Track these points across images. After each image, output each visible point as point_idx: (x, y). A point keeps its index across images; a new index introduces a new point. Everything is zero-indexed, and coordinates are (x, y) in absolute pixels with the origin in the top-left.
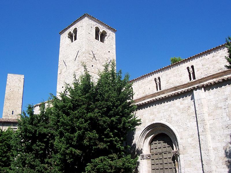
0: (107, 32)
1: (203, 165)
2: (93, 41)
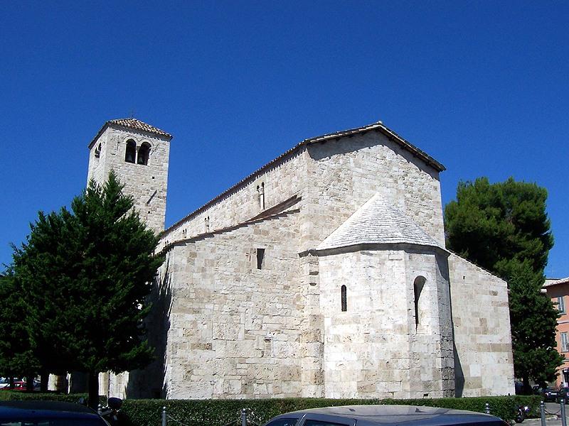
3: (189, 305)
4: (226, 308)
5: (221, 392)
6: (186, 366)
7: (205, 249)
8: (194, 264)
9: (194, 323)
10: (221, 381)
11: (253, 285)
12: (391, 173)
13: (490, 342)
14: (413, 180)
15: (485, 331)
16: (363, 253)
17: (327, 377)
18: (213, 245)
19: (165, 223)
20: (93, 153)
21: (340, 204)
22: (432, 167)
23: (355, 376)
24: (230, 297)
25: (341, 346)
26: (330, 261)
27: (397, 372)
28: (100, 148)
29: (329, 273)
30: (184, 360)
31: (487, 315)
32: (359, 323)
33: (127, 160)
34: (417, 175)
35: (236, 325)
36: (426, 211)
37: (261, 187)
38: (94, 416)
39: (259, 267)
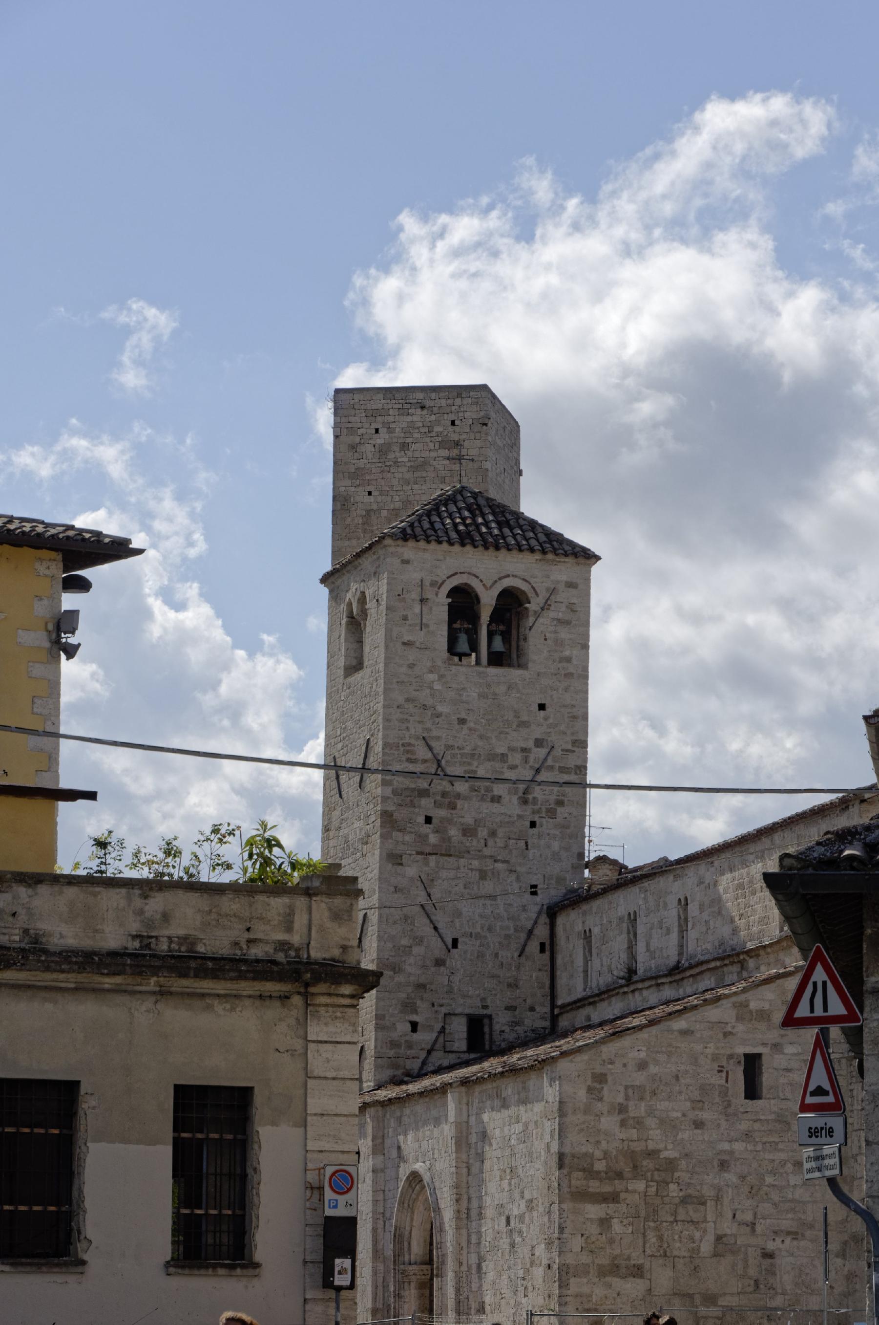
0: (524, 587)
3: (595, 1186)
7: (625, 1065)
8: (601, 1099)
9: (605, 1223)
18: (643, 1055)
33: (452, 649)
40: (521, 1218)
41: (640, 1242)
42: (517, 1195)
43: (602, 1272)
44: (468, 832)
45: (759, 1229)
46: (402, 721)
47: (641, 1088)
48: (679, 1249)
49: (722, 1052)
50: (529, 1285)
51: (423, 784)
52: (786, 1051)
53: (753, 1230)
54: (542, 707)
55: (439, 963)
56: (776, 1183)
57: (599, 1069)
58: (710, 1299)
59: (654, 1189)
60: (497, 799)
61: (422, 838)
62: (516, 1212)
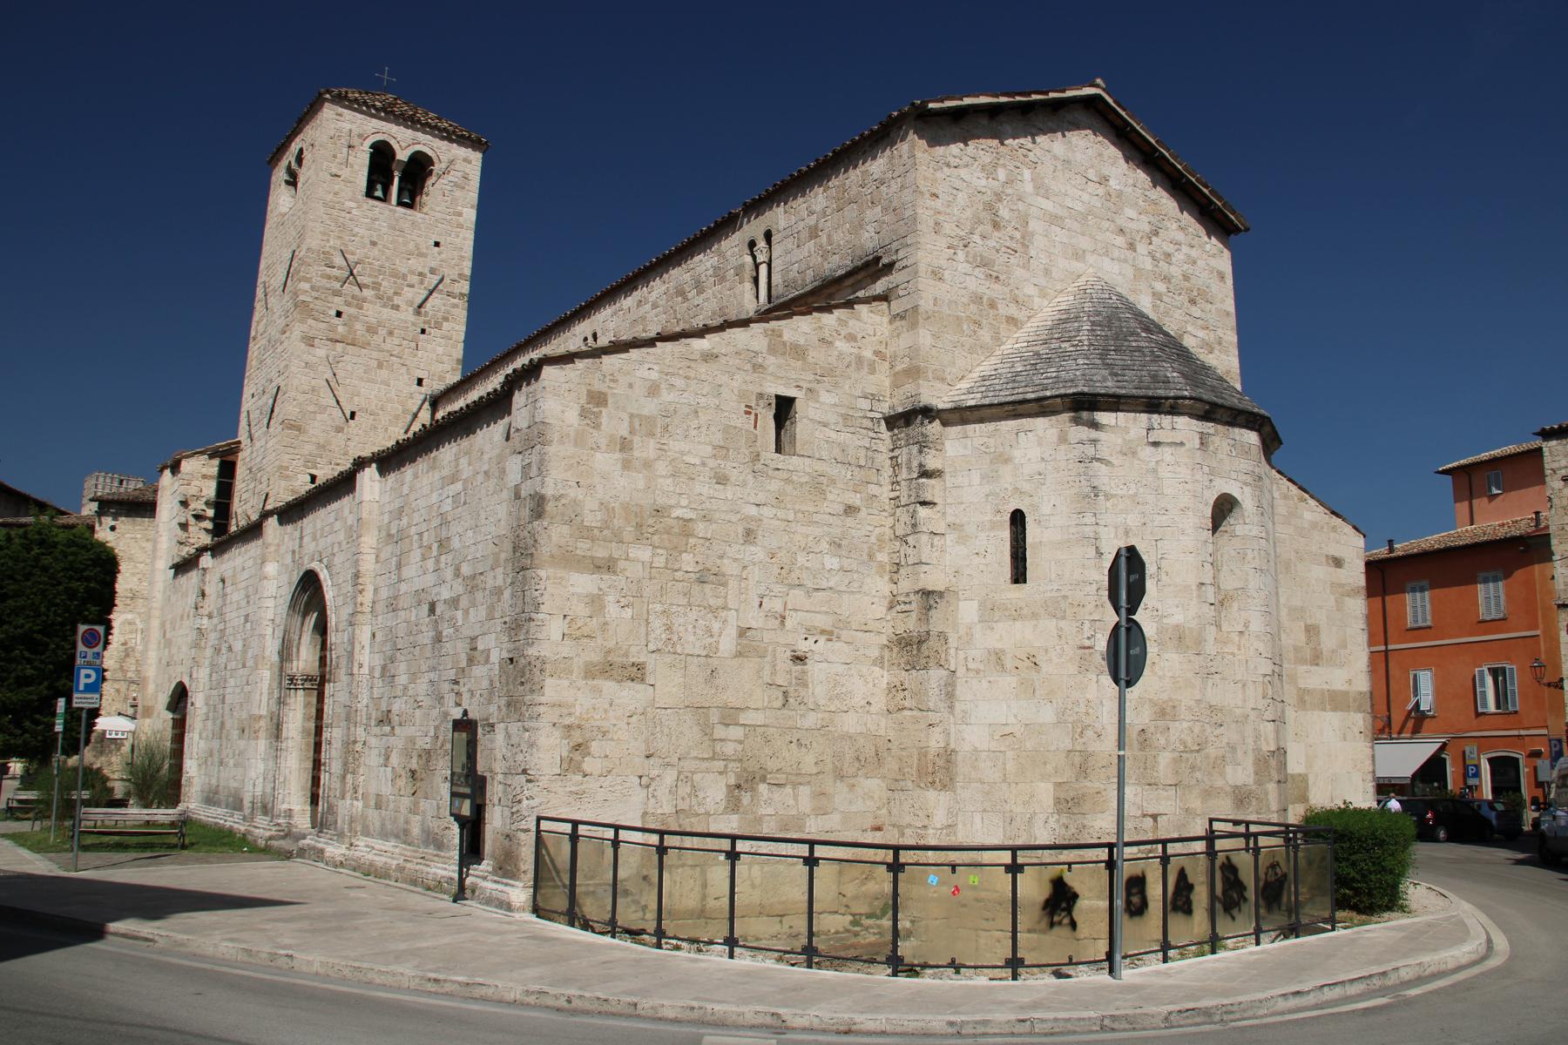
0: (430, 153)
1: (701, 332)
2: (353, 205)
3: (583, 547)
4: (688, 561)
5: (668, 809)
6: (569, 727)
7: (631, 386)
8: (597, 426)
9: (596, 602)
10: (670, 777)
11: (761, 498)
12: (1121, 221)
13: (1326, 687)
14: (1170, 248)
15: (1316, 659)
16: (1077, 421)
17: (962, 769)
18: (654, 375)
19: (466, 361)
20: (280, 175)
21: (996, 291)
22: (1217, 222)
23: (1049, 768)
24: (700, 528)
25: (1009, 681)
26: (977, 442)
27: (1165, 759)
28: (299, 160)
29: (976, 479)
30: (565, 711)
31: (1319, 618)
32: (1064, 618)
33: (370, 193)
34: (1180, 236)
35: (713, 611)
36: (1201, 334)
37: (762, 244)
38: (456, 974)
39: (778, 450)
40: (454, 602)
41: (643, 630)
42: (449, 574)
43: (590, 672)
44: (371, 330)
45: (788, 622)
46: (324, 234)
47: (649, 420)
48: (692, 643)
49: (751, 387)
50: (463, 690)
51: (337, 285)
52: (822, 399)
53: (782, 623)
54: (437, 244)
55: (339, 430)
56: (808, 565)
57: (598, 386)
58: (730, 716)
59: (662, 559)
60: (396, 308)
61: (333, 329)
62: (446, 594)
